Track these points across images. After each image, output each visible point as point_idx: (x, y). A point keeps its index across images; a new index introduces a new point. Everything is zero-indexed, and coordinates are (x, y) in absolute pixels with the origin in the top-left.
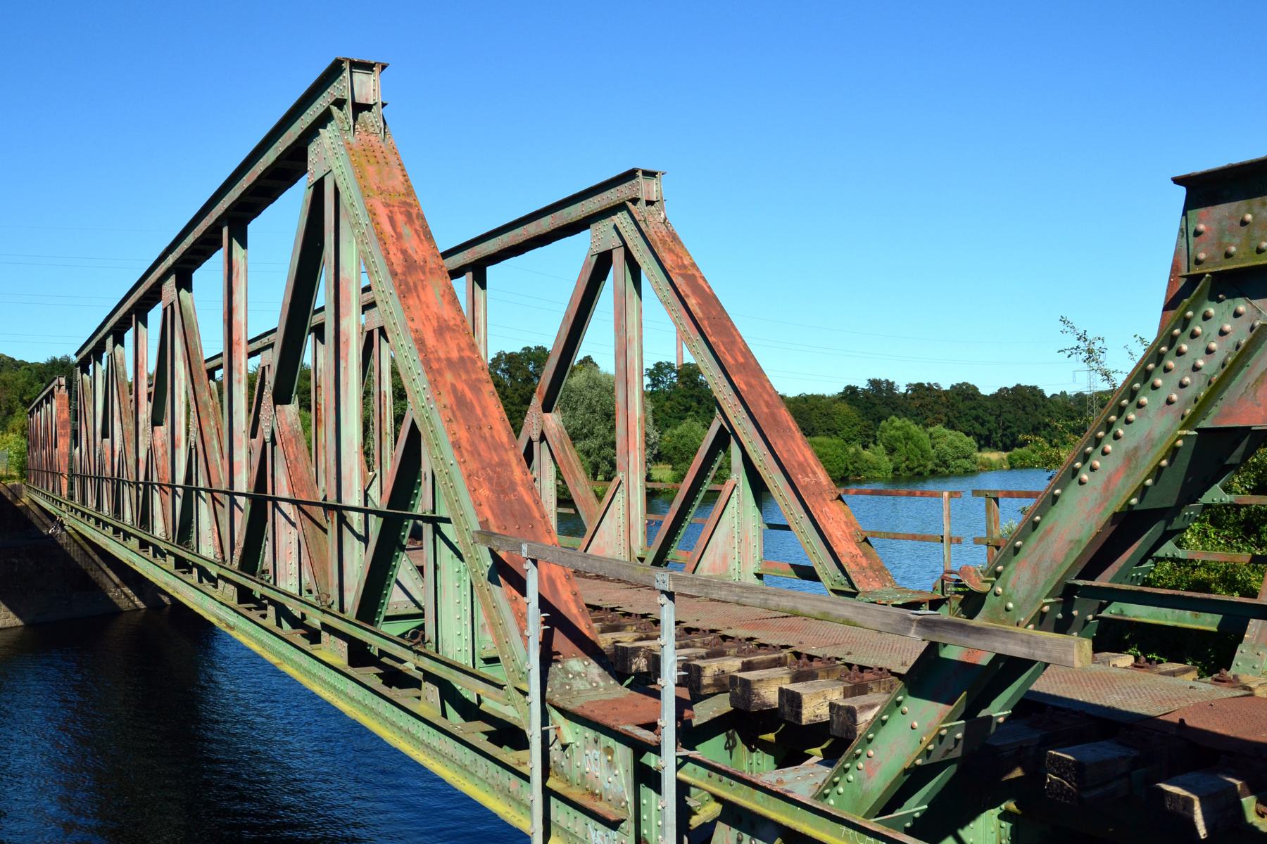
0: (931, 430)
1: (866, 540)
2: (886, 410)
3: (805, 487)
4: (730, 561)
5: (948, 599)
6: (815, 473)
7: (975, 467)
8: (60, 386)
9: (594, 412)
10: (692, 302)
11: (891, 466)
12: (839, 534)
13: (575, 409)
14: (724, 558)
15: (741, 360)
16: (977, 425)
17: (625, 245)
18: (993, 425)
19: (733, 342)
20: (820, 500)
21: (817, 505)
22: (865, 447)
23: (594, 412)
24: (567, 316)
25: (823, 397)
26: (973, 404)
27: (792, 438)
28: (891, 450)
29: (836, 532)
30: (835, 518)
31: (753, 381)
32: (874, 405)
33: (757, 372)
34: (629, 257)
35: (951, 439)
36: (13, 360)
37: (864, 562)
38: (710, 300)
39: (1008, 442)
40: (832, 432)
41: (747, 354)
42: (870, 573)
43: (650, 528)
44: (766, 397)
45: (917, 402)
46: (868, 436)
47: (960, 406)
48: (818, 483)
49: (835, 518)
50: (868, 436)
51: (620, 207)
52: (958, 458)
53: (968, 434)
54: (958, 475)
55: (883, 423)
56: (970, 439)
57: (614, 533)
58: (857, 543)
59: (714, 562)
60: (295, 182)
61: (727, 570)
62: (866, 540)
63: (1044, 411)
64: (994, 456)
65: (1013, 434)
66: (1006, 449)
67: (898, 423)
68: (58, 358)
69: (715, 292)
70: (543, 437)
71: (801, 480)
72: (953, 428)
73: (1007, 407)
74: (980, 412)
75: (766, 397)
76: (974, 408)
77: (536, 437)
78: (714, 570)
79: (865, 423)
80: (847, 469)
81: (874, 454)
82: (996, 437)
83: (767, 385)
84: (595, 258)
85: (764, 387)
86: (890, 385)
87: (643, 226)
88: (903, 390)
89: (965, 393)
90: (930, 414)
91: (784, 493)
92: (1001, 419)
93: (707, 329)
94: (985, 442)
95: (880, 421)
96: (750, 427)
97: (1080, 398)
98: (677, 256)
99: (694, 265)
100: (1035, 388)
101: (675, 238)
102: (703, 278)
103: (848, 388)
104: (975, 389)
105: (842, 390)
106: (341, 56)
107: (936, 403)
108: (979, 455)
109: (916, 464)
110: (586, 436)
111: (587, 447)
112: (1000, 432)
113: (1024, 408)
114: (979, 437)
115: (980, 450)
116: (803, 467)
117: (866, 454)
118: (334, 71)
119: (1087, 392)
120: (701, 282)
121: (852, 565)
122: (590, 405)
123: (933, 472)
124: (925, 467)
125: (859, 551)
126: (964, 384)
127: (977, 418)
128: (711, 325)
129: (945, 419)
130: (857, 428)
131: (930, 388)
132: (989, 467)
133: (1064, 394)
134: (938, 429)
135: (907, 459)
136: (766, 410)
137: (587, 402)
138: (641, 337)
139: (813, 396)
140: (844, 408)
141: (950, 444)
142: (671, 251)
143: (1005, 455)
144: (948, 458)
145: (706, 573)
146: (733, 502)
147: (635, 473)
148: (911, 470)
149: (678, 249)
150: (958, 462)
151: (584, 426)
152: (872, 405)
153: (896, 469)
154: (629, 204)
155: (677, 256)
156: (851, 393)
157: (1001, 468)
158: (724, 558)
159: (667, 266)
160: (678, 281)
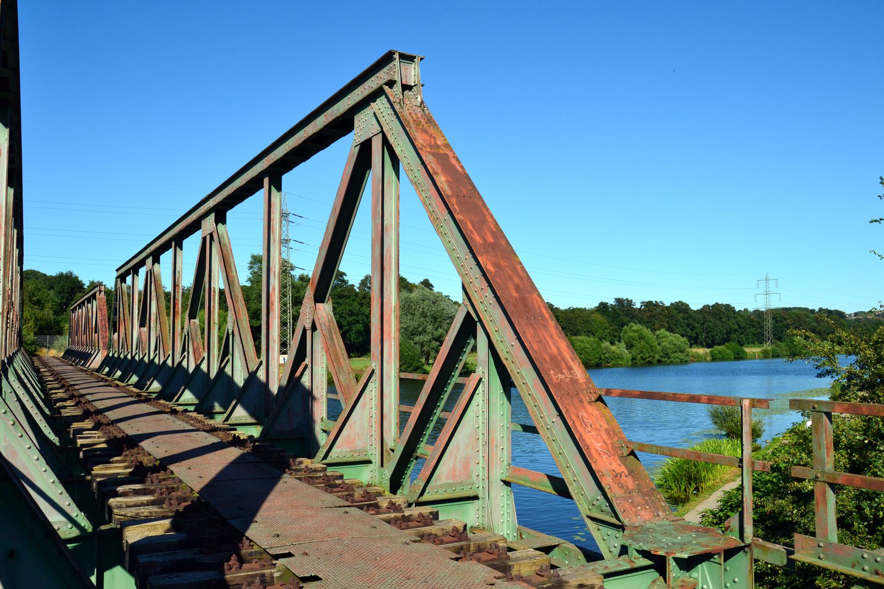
0: (658, 332)
1: (632, 453)
2: (626, 319)
3: (559, 386)
4: (472, 466)
5: (748, 546)
6: (570, 369)
7: (687, 359)
8: (100, 292)
9: (426, 316)
10: (441, 180)
11: (630, 356)
12: (598, 445)
13: (414, 314)
14: (466, 463)
15: (490, 239)
16: (688, 330)
17: (382, 132)
18: (699, 330)
19: (484, 221)
20: (576, 402)
21: (572, 409)
22: (612, 343)
23: (426, 316)
24: (334, 209)
25: (585, 309)
26: (686, 315)
27: (545, 327)
28: (630, 346)
29: (594, 442)
30: (594, 425)
31: (502, 262)
32: (619, 315)
33: (509, 253)
34: (386, 142)
35: (672, 339)
36: (45, 275)
37: (630, 483)
38: (461, 179)
39: (710, 342)
40: (590, 333)
41: (498, 233)
42: (638, 499)
43: (403, 417)
44: (516, 280)
45: (648, 314)
46: (615, 336)
47: (676, 316)
48: (574, 381)
49: (594, 425)
50: (615, 336)
51: (378, 93)
52: (676, 352)
53: (683, 336)
54: (675, 364)
55: (625, 327)
56: (685, 339)
57: (366, 424)
58: (622, 458)
59: (454, 469)
60: (309, 158)
61: (469, 477)
62: (632, 453)
63: (734, 321)
64: (701, 351)
65: (713, 336)
66: (708, 346)
67: (635, 327)
68: (64, 272)
69: (468, 172)
70: (314, 328)
71: (554, 377)
72: (672, 331)
73: (709, 318)
74: (691, 321)
75: (516, 280)
76: (687, 319)
77: (308, 326)
78: (454, 477)
79: (613, 328)
80: (600, 358)
81: (620, 348)
82: (702, 337)
83: (519, 267)
84: (358, 148)
85: (514, 269)
86: (630, 302)
87: (397, 107)
88: (638, 306)
89: (681, 308)
90: (657, 322)
91: (533, 391)
92: (705, 326)
93: (455, 207)
94: (694, 341)
95: (623, 326)
96: (498, 313)
97: (757, 313)
98: (431, 136)
99: (447, 146)
100: (728, 306)
101: (430, 120)
102: (458, 160)
103: (601, 304)
104: (687, 306)
105: (597, 305)
106: (393, 49)
107: (660, 314)
108: (689, 350)
109: (647, 355)
110: (421, 333)
111: (421, 340)
112: (704, 335)
113: (720, 319)
114: (690, 338)
115: (691, 347)
116: (557, 362)
117: (613, 348)
118: (387, 59)
119: (762, 309)
120: (453, 161)
121: (615, 488)
122: (423, 312)
123: (659, 362)
124: (653, 357)
125: (623, 469)
126: (680, 302)
127: (688, 325)
128: (459, 203)
129: (667, 325)
130: (607, 331)
131: (656, 305)
132: (698, 359)
133: (746, 310)
134: (663, 332)
135: (641, 352)
136: (515, 294)
137: (421, 310)
138: (398, 225)
139: (578, 309)
140: (599, 317)
141: (671, 343)
142: (425, 131)
143: (708, 350)
144: (669, 351)
145: (444, 481)
146: (478, 399)
147: (389, 362)
148: (644, 359)
149: (432, 130)
150: (676, 355)
151: (419, 326)
152: (618, 315)
153: (633, 359)
154: (386, 88)
155: (431, 136)
156: (603, 307)
157: (705, 359)
158: (466, 463)
159: (418, 144)
160: (429, 159)
